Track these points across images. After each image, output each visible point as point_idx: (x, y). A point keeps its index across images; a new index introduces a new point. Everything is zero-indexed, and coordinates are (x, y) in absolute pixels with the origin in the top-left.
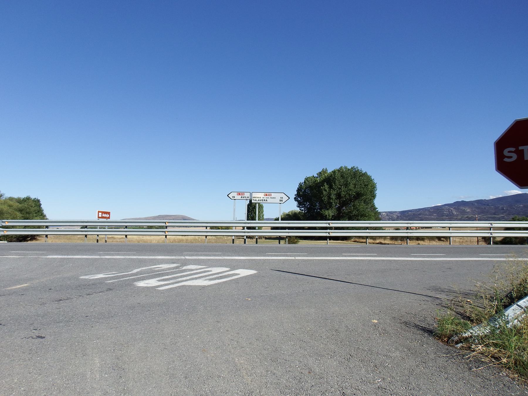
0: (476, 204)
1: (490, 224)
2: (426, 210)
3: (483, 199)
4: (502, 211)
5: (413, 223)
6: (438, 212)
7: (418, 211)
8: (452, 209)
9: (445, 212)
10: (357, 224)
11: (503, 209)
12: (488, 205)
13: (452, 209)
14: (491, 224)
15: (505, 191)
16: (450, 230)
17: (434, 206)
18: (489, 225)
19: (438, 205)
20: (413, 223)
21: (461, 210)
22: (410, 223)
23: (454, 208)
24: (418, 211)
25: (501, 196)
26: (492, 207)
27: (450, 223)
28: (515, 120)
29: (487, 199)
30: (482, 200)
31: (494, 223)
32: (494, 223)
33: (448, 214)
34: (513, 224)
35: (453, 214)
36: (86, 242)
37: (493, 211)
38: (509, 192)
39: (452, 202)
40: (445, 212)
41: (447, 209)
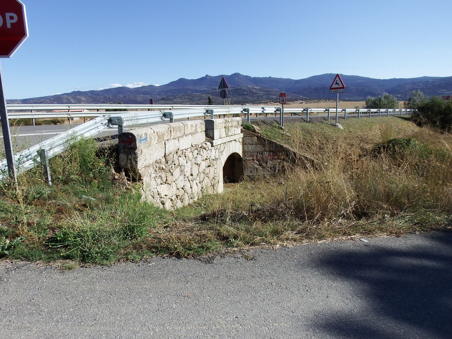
0: (89, 94)
1: (68, 107)
2: (47, 98)
3: (95, 90)
4: (109, 100)
5: (130, 106)
6: (58, 100)
7: (39, 100)
8: (70, 98)
9: (64, 101)
10: (116, 107)
11: (110, 98)
12: (98, 95)
13: (70, 98)
14: (69, 106)
15: (110, 84)
16: (32, 112)
17: (53, 95)
18: (67, 108)
19: (57, 94)
20: (130, 106)
21: (78, 98)
22: (128, 106)
23: (72, 97)
24: (39, 100)
25: (107, 88)
26: (102, 97)
27: (127, 106)
28: (222, 169)
29: (98, 90)
30: (94, 91)
31: (71, 106)
32: (71, 106)
33: (67, 102)
34: (87, 107)
35: (71, 102)
36: (163, 110)
37: (103, 100)
38: (113, 85)
39: (70, 92)
40: (64, 101)
41: (66, 98)
